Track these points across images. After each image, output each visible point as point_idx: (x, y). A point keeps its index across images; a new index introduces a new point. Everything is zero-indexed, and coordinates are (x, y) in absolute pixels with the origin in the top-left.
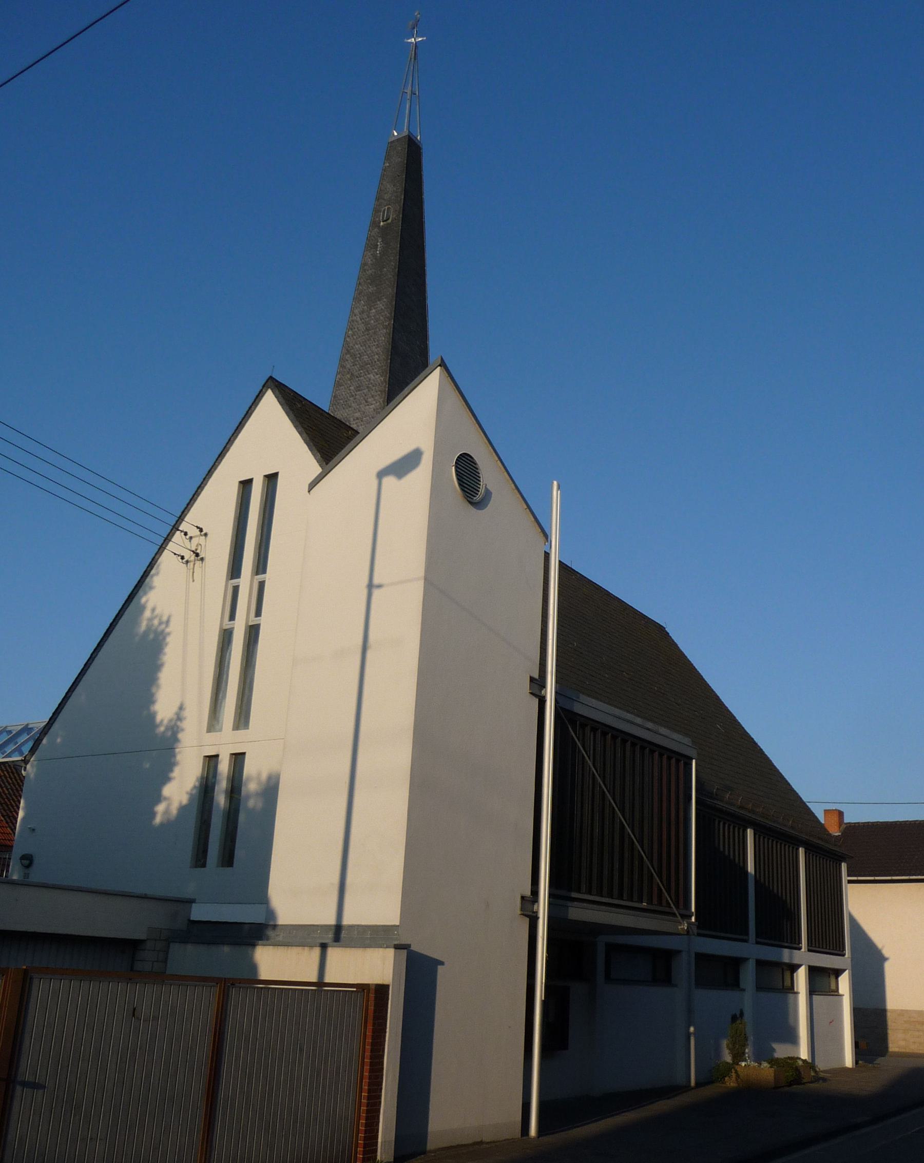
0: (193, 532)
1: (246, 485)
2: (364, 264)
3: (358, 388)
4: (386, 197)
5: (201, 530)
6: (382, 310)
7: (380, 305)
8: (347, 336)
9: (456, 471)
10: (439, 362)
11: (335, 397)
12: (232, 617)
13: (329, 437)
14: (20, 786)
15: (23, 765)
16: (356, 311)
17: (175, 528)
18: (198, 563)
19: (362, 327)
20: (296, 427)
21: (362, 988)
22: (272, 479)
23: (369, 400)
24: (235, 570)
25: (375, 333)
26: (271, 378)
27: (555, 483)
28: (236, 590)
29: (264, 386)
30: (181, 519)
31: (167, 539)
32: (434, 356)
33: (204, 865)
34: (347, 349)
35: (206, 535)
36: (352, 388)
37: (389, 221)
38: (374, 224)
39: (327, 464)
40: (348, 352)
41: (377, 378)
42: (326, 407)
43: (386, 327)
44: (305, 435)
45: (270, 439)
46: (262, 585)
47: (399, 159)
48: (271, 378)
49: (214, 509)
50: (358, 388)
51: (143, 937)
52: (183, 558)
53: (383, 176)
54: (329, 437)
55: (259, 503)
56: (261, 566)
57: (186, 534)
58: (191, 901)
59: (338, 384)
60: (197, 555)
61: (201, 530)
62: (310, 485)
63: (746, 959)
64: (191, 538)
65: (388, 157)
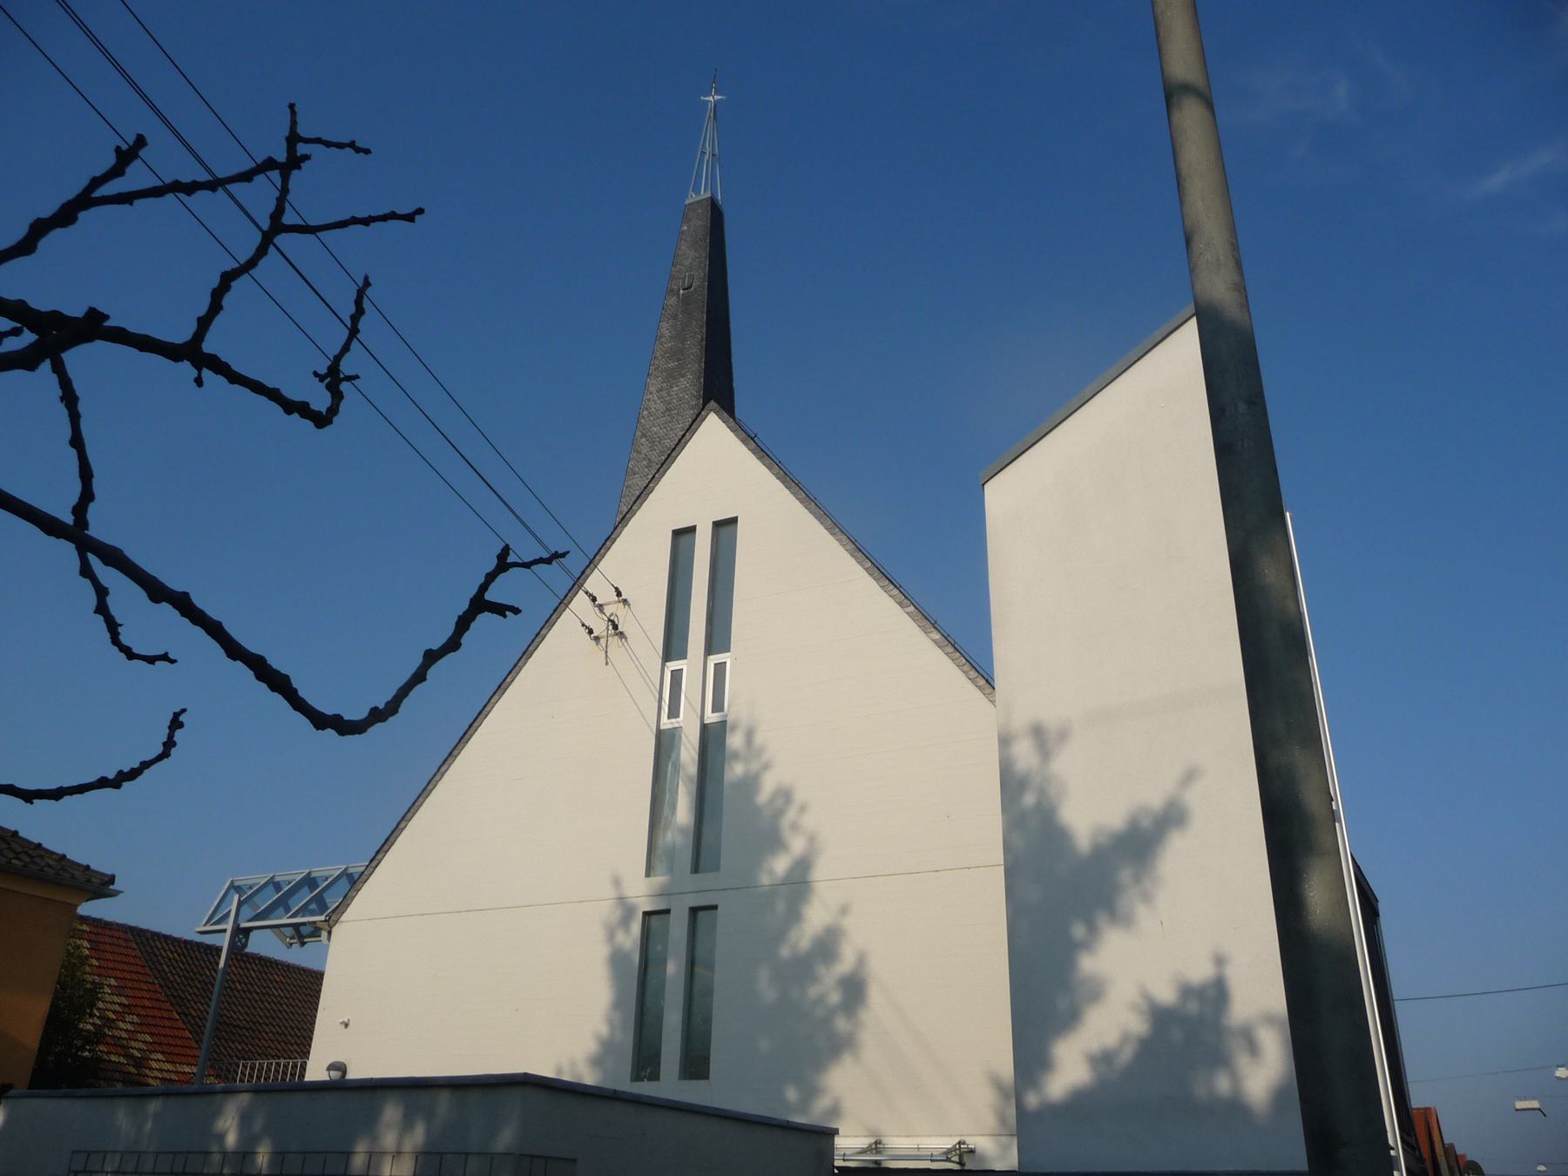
0: (605, 595)
1: (683, 535)
4: (687, 262)
5: (619, 594)
12: (674, 712)
15: (325, 926)
17: (577, 583)
18: (614, 641)
22: (725, 527)
24: (673, 647)
28: (677, 676)
30: (592, 563)
46: (720, 668)
47: (701, 222)
49: (634, 563)
52: (591, 632)
56: (717, 639)
61: (619, 594)
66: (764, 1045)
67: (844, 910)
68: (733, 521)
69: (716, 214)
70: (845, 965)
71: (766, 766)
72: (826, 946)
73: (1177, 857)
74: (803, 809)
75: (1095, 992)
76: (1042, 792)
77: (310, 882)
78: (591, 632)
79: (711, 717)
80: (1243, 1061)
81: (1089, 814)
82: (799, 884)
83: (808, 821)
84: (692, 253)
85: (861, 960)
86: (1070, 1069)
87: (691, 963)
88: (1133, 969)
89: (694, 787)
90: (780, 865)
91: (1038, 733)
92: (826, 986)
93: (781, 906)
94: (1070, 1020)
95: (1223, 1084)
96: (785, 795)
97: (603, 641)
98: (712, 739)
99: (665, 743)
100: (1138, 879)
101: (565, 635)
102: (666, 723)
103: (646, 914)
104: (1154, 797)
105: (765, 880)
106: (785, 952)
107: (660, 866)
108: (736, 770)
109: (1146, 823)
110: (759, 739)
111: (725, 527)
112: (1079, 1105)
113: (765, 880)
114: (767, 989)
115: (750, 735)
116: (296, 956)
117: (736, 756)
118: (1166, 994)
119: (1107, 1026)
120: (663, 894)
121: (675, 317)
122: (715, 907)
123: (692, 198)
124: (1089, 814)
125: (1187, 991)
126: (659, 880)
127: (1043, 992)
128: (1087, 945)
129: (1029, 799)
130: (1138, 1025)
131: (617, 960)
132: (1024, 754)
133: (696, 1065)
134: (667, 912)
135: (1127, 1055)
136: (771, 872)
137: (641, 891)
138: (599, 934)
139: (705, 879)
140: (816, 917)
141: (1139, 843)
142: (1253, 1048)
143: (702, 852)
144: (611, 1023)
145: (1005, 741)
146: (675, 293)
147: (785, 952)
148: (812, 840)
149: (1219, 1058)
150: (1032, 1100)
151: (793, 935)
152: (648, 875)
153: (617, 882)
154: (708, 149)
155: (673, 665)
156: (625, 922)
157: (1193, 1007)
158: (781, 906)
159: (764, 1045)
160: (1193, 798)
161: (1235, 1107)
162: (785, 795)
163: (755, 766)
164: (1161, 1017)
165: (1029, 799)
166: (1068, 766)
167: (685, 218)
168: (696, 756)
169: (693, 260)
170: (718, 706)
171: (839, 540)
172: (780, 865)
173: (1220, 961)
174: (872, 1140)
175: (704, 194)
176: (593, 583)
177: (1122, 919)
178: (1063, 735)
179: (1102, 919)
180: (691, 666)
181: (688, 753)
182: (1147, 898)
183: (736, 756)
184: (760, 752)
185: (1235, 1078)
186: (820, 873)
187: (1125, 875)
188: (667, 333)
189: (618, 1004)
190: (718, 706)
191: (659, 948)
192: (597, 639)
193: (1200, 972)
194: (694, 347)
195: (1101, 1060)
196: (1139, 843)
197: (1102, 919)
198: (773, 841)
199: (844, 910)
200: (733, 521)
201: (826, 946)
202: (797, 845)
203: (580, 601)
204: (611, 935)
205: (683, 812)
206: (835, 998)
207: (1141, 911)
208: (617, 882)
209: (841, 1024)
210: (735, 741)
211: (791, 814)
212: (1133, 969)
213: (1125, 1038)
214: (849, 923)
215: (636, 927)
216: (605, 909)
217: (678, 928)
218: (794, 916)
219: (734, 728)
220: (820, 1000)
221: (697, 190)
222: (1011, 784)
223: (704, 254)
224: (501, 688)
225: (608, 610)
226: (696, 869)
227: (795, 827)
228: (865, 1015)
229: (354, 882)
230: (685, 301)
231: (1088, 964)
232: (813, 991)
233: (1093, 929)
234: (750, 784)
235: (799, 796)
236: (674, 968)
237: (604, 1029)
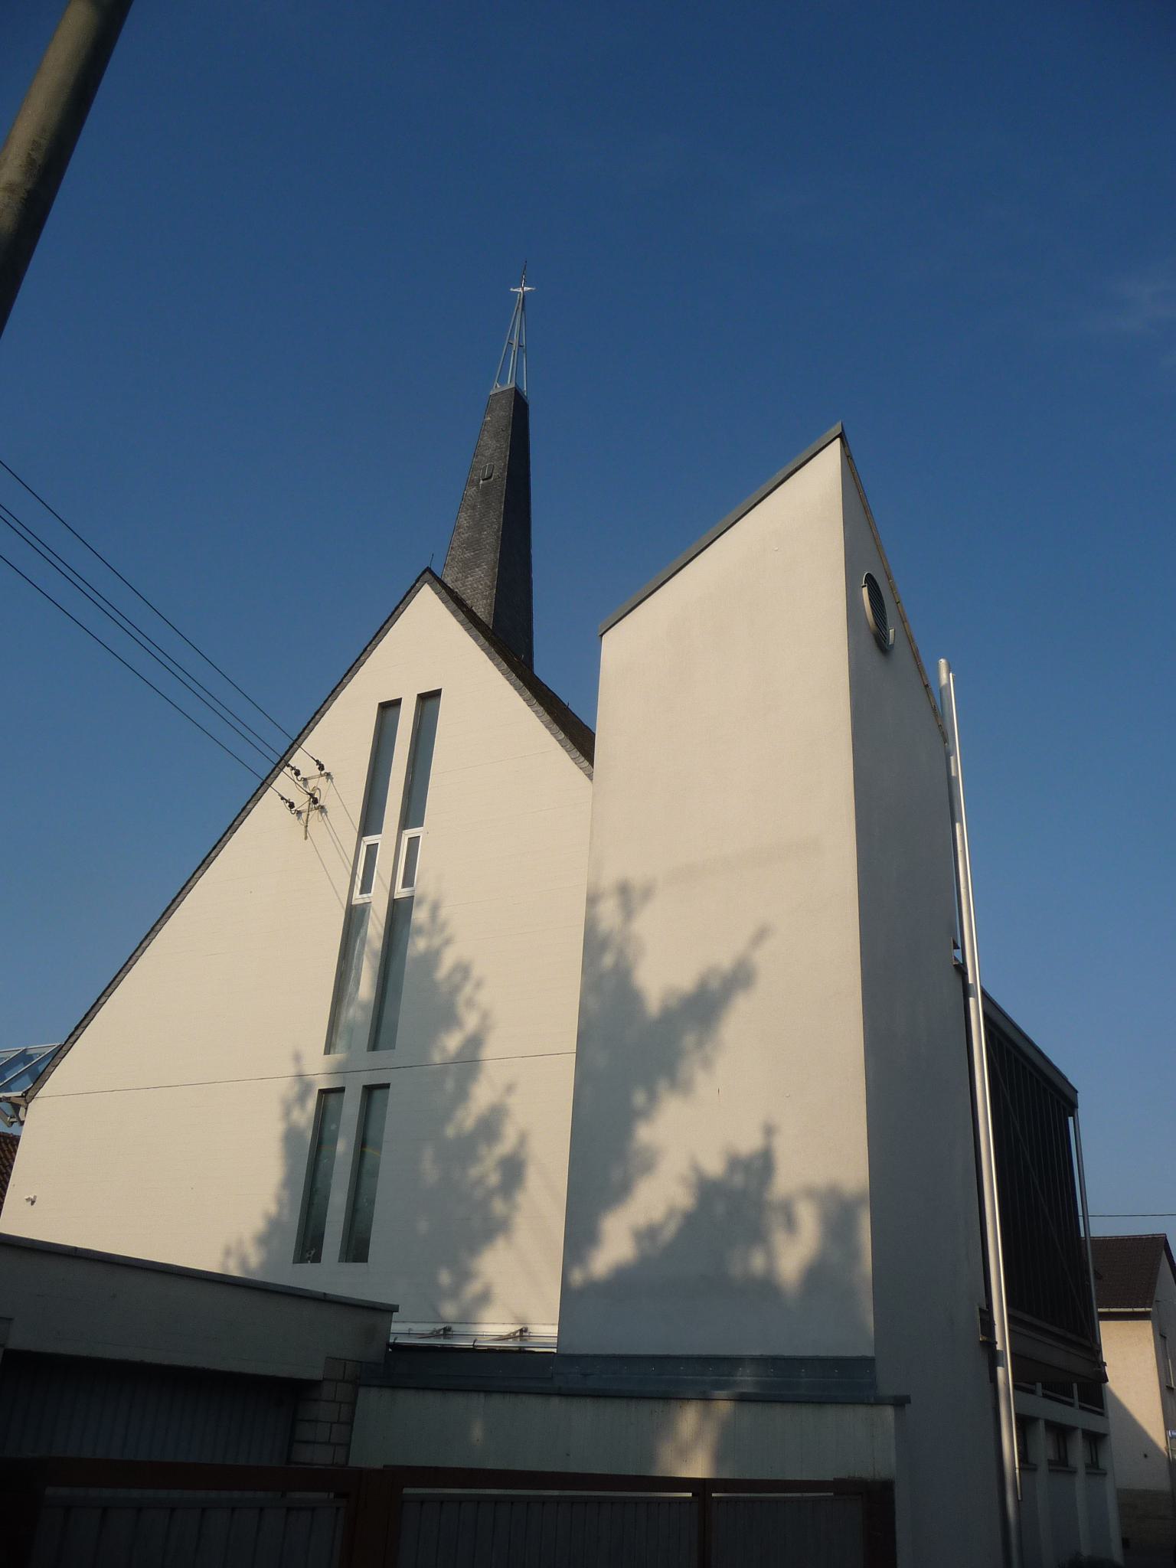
0: (308, 769)
1: (389, 708)
4: (488, 453)
5: (321, 768)
12: (366, 888)
15: (22, 1103)
17: (283, 761)
18: (315, 814)
21: (844, 1488)
22: (429, 699)
24: (370, 822)
27: (943, 661)
28: (372, 849)
30: (295, 743)
31: (265, 783)
33: (317, 1259)
35: (328, 775)
45: (429, 646)
46: (414, 842)
47: (503, 413)
48: (428, 570)
49: (341, 738)
51: (317, 1374)
52: (292, 805)
55: (412, 730)
56: (412, 814)
57: (297, 773)
58: (391, 1310)
60: (315, 801)
61: (321, 768)
63: (1075, 1429)
64: (305, 780)
66: (423, 1226)
67: (510, 1089)
68: (436, 694)
69: (520, 406)
70: (506, 1146)
71: (448, 942)
72: (490, 1126)
73: (740, 1023)
74: (479, 985)
75: (648, 1164)
76: (621, 953)
77: (24, 1057)
78: (292, 805)
79: (401, 892)
80: (779, 1238)
81: (662, 975)
82: (469, 1062)
83: (484, 997)
84: (493, 444)
85: (523, 1139)
86: (616, 1246)
87: (362, 1143)
88: (686, 1139)
89: (377, 963)
90: (453, 1042)
91: (624, 891)
92: (487, 1169)
93: (450, 1085)
94: (618, 1192)
95: (758, 1262)
96: (463, 970)
97: (304, 816)
98: (399, 912)
99: (355, 917)
100: (700, 1044)
101: (268, 810)
102: (358, 899)
103: (320, 1091)
104: (724, 958)
105: (437, 1058)
106: (450, 1131)
107: (340, 1043)
108: (418, 945)
109: (715, 984)
110: (444, 913)
111: (429, 699)
112: (622, 1281)
113: (437, 1058)
114: (430, 1170)
115: (435, 908)
116: (12, 1131)
117: (420, 931)
118: (714, 1166)
119: (657, 1198)
120: (339, 1071)
121: (474, 507)
122: (387, 1086)
123: (497, 388)
124: (662, 975)
125: (735, 1163)
126: (337, 1056)
127: (601, 1164)
128: (644, 1114)
129: (608, 960)
130: (683, 1198)
131: (291, 1136)
132: (609, 912)
133: (356, 1249)
134: (341, 1090)
135: (670, 1231)
136: (444, 1050)
137: (319, 1068)
138: (275, 1110)
139: (381, 1057)
140: (482, 1096)
141: (704, 1006)
142: (791, 1224)
143: (380, 1029)
144: (280, 1202)
145: (592, 900)
146: (472, 483)
147: (450, 1131)
148: (485, 1017)
149: (757, 1235)
150: (577, 1277)
151: (460, 1114)
152: (327, 1051)
153: (297, 1058)
154: (515, 342)
155: (369, 840)
156: (302, 1098)
157: (739, 1180)
158: (450, 1085)
159: (423, 1226)
160: (763, 959)
161: (767, 1287)
162: (463, 970)
163: (437, 941)
164: (708, 1191)
165: (608, 960)
166: (648, 925)
167: (489, 409)
168: (381, 931)
169: (494, 452)
170: (408, 882)
171: (536, 712)
172: (453, 1042)
173: (769, 1131)
174: (519, 1327)
175: (510, 385)
176: (298, 759)
177: (681, 1086)
178: (648, 893)
179: (662, 1085)
180: (385, 839)
181: (375, 928)
182: (707, 1064)
183: (420, 931)
184: (443, 926)
185: (770, 1256)
186: (490, 1051)
187: (689, 1040)
188: (465, 524)
189: (288, 1182)
190: (408, 882)
191: (333, 1127)
192: (299, 813)
193: (749, 1142)
194: (490, 537)
195: (646, 1235)
196: (704, 1006)
197: (662, 1085)
198: (449, 1018)
199: (510, 1089)
200: (436, 694)
201: (490, 1126)
202: (471, 1021)
203: (283, 782)
204: (287, 1113)
205: (365, 988)
206: (494, 1179)
207: (700, 1078)
208: (297, 1058)
209: (498, 1206)
210: (420, 915)
211: (468, 989)
212: (686, 1139)
213: (671, 1213)
214: (514, 1102)
215: (311, 1104)
216: (284, 1086)
217: (351, 1107)
218: (462, 1094)
219: (420, 903)
220: (480, 1181)
221: (503, 382)
222: (594, 943)
223: (505, 445)
224: (205, 863)
225: (312, 784)
226: (374, 1045)
227: (470, 1003)
228: (521, 1198)
229: (57, 1055)
230: (485, 492)
231: (645, 1134)
232: (474, 1172)
233: (653, 1098)
234: (432, 958)
235: (476, 972)
236: (343, 1147)
237: (273, 1208)
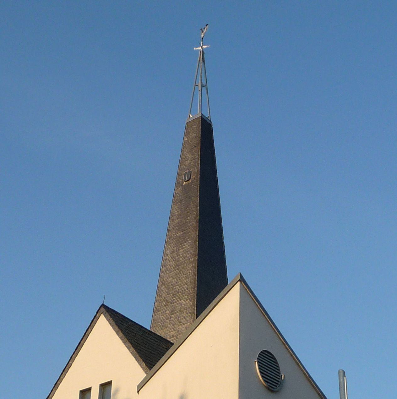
2: (172, 216)
3: (172, 312)
4: (187, 163)
6: (189, 250)
7: (186, 246)
8: (161, 271)
9: (259, 365)
10: (239, 278)
11: (154, 320)
13: (150, 348)
14: (279, 373)
16: (168, 252)
19: (173, 264)
20: (124, 343)
22: (106, 387)
23: (182, 321)
25: (183, 268)
26: (103, 305)
29: (97, 313)
32: (232, 274)
34: (162, 282)
36: (167, 312)
37: (190, 181)
38: (178, 184)
39: (150, 370)
40: (163, 284)
41: (188, 303)
42: (147, 325)
43: (192, 263)
44: (132, 349)
47: (196, 134)
48: (103, 305)
50: (172, 312)
53: (183, 148)
54: (150, 348)
59: (156, 311)
62: (138, 386)
65: (187, 134)
